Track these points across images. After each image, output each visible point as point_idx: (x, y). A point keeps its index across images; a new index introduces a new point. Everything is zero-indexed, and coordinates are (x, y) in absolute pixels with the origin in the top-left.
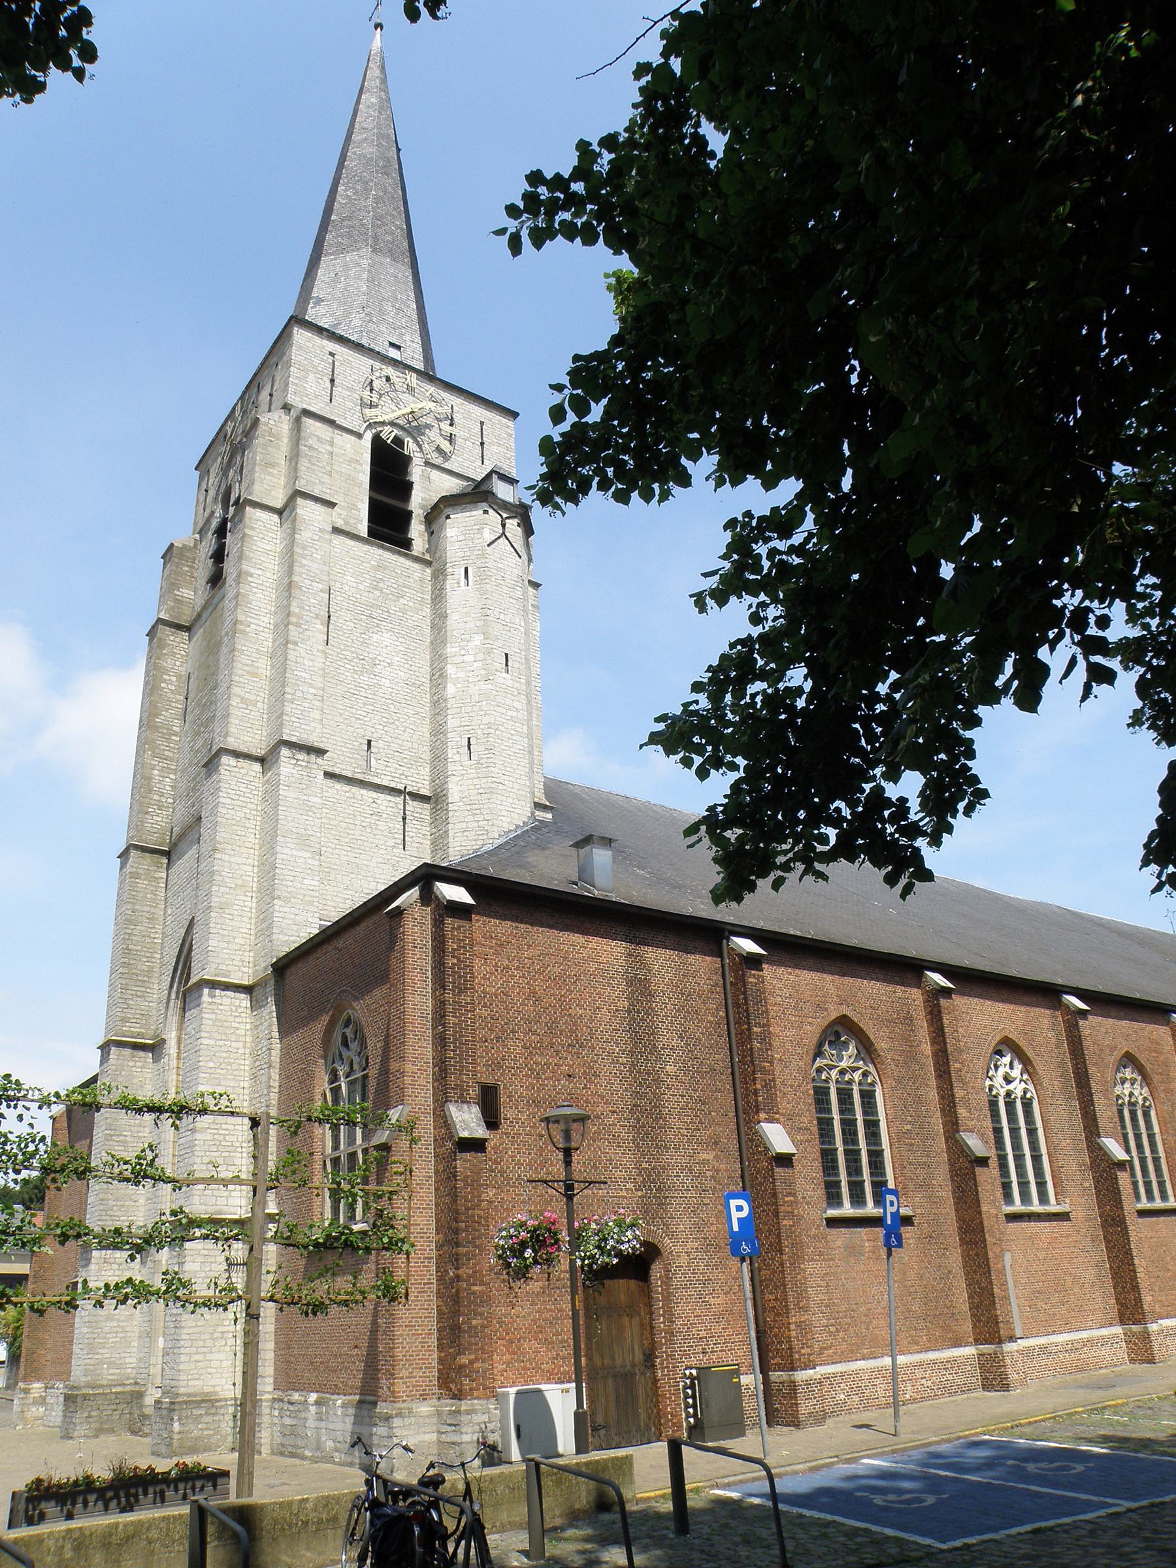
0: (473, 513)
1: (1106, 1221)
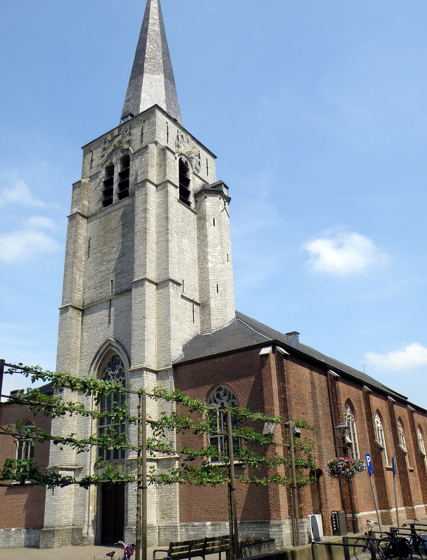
0: (216, 198)
1: (400, 472)
